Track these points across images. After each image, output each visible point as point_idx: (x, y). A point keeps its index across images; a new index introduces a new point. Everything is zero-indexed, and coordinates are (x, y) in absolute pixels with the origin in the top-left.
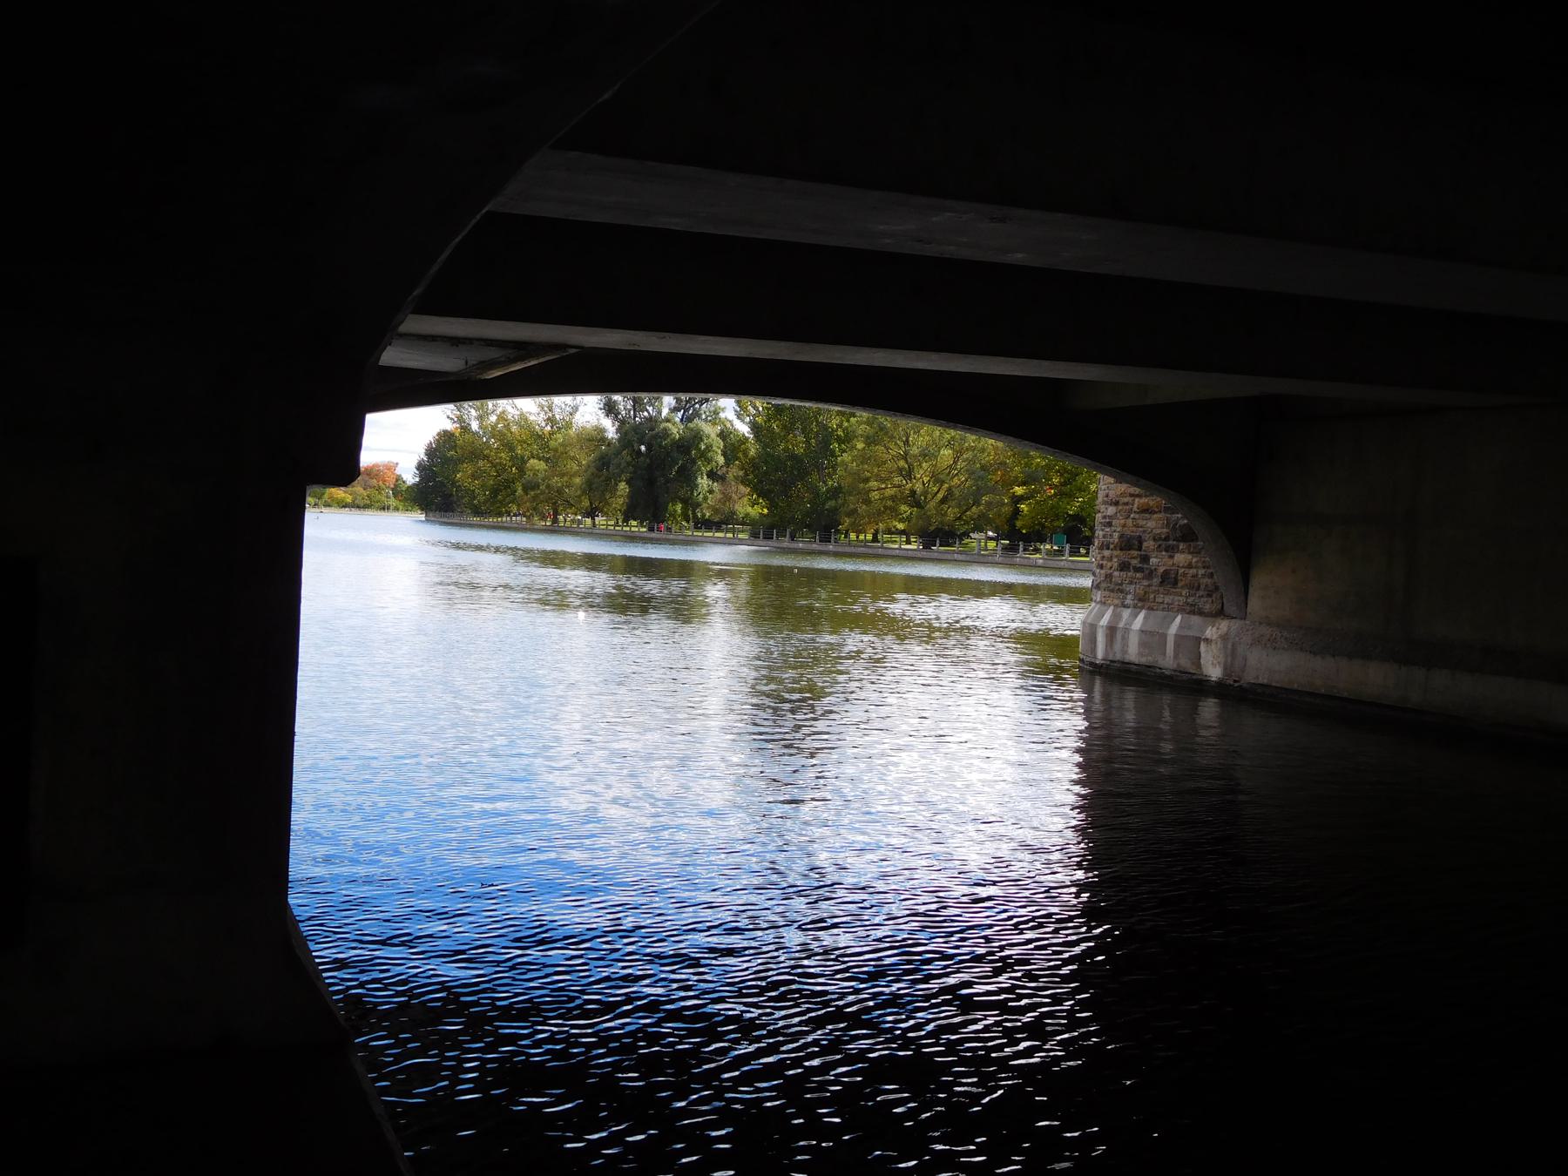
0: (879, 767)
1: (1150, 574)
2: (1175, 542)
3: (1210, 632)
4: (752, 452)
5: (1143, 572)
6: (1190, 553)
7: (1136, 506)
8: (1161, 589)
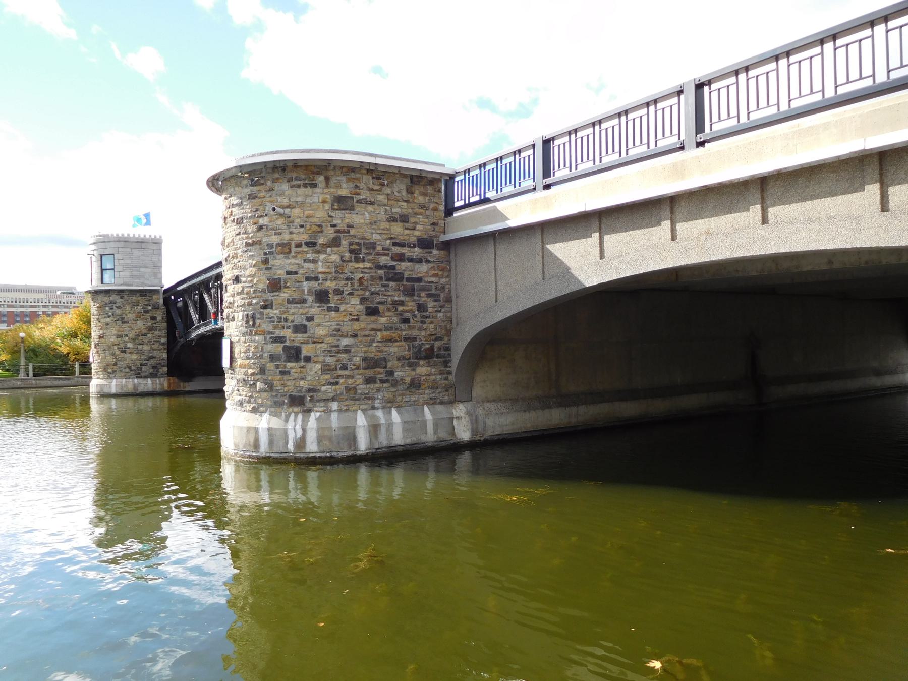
1: (395, 384)
2: (416, 360)
3: (456, 413)
4: (195, 609)
5: (389, 382)
6: (429, 366)
8: (407, 392)
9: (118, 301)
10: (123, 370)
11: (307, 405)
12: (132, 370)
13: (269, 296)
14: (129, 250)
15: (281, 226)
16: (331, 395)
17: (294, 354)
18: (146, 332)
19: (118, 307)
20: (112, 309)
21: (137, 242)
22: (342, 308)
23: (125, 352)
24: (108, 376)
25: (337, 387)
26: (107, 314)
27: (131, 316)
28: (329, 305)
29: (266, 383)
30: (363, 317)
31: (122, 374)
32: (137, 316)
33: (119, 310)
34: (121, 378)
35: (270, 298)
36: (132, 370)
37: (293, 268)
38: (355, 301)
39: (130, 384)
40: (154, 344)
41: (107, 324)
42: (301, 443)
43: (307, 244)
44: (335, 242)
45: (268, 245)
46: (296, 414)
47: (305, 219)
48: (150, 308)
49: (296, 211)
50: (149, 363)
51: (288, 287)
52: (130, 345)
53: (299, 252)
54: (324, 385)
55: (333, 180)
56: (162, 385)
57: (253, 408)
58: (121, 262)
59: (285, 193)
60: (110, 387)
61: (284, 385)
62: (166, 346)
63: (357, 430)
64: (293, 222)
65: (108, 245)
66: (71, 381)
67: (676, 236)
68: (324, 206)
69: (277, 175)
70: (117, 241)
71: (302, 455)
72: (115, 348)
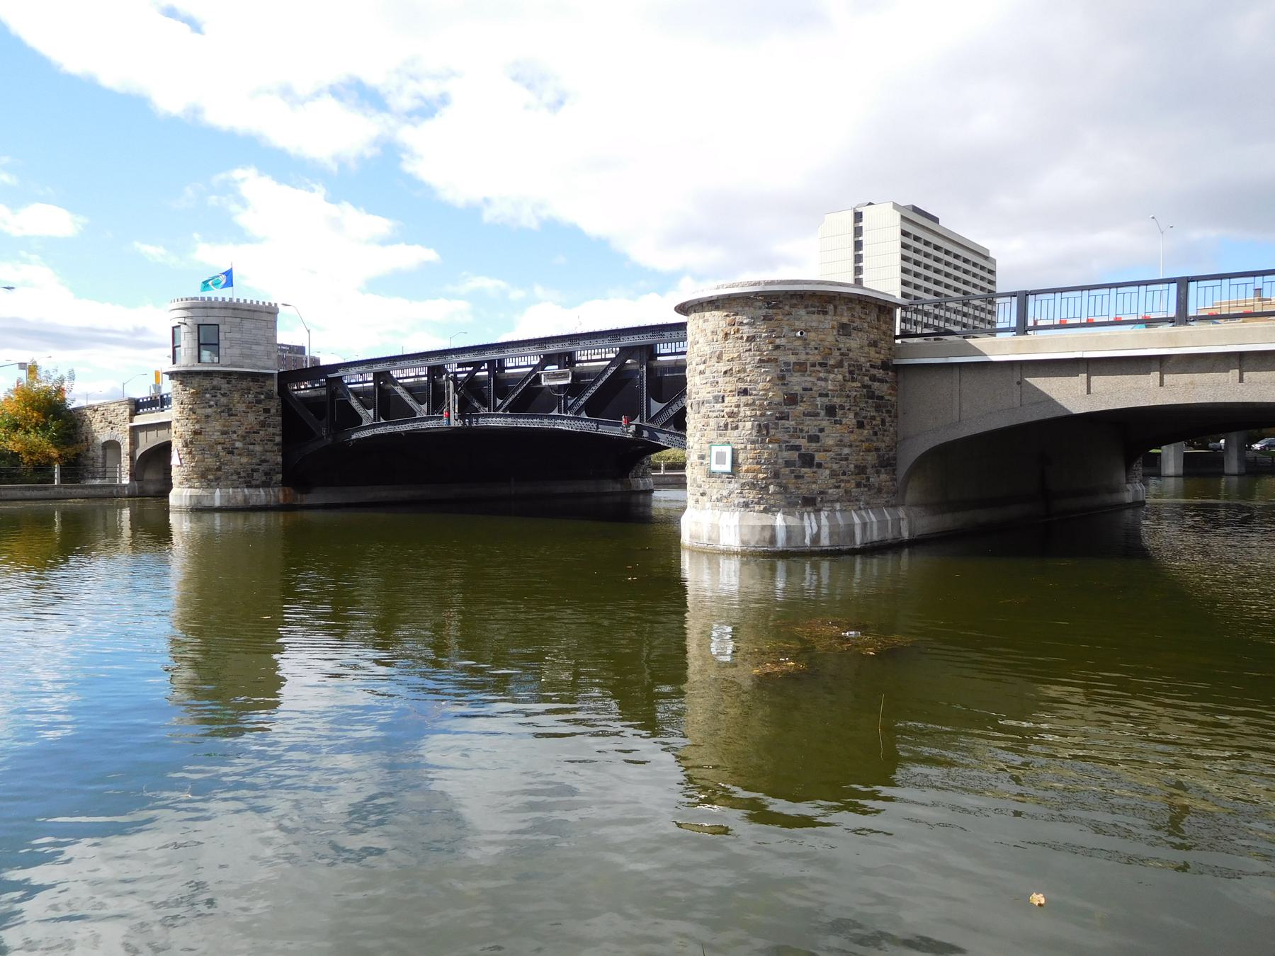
0: (294, 755)
6: (886, 474)
7: (864, 447)
8: (875, 496)
9: (223, 386)
10: (230, 477)
11: (818, 505)
12: (242, 477)
13: (785, 409)
14: (238, 320)
15: (798, 348)
16: (836, 497)
17: (808, 460)
18: (258, 428)
19: (224, 395)
20: (215, 396)
21: (249, 310)
22: (844, 421)
23: (232, 453)
24: (208, 484)
25: (840, 490)
26: (206, 403)
27: (241, 407)
28: (836, 419)
29: (781, 487)
30: (855, 430)
31: (229, 482)
32: (248, 407)
33: (225, 398)
34: (227, 487)
35: (786, 410)
36: (242, 477)
37: (808, 385)
38: (851, 415)
39: (239, 495)
40: (266, 444)
41: (207, 416)
42: (816, 538)
43: (821, 364)
44: (840, 365)
45: (784, 363)
46: (809, 513)
47: (819, 343)
48: (262, 397)
49: (812, 335)
50: (262, 468)
51: (805, 402)
52: (238, 444)
53: (814, 371)
54: (831, 488)
55: (839, 309)
56: (277, 497)
57: (765, 509)
58: (228, 335)
59: (803, 318)
60: (213, 498)
61: (798, 488)
62: (280, 447)
63: (856, 526)
64: (809, 344)
65: (210, 312)
66: (50, 491)
67: (1163, 383)
68: (833, 332)
69: (794, 301)
70: (224, 308)
71: (816, 549)
72: (220, 447)
